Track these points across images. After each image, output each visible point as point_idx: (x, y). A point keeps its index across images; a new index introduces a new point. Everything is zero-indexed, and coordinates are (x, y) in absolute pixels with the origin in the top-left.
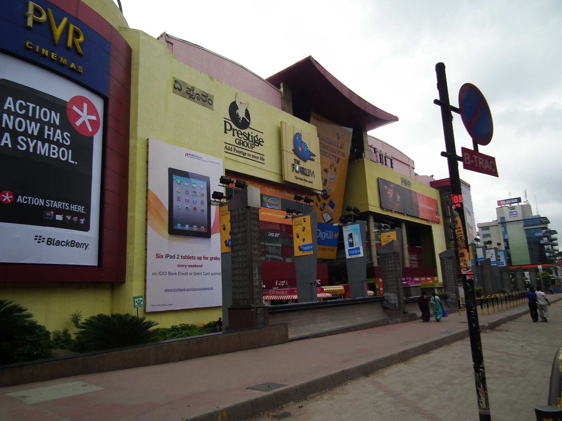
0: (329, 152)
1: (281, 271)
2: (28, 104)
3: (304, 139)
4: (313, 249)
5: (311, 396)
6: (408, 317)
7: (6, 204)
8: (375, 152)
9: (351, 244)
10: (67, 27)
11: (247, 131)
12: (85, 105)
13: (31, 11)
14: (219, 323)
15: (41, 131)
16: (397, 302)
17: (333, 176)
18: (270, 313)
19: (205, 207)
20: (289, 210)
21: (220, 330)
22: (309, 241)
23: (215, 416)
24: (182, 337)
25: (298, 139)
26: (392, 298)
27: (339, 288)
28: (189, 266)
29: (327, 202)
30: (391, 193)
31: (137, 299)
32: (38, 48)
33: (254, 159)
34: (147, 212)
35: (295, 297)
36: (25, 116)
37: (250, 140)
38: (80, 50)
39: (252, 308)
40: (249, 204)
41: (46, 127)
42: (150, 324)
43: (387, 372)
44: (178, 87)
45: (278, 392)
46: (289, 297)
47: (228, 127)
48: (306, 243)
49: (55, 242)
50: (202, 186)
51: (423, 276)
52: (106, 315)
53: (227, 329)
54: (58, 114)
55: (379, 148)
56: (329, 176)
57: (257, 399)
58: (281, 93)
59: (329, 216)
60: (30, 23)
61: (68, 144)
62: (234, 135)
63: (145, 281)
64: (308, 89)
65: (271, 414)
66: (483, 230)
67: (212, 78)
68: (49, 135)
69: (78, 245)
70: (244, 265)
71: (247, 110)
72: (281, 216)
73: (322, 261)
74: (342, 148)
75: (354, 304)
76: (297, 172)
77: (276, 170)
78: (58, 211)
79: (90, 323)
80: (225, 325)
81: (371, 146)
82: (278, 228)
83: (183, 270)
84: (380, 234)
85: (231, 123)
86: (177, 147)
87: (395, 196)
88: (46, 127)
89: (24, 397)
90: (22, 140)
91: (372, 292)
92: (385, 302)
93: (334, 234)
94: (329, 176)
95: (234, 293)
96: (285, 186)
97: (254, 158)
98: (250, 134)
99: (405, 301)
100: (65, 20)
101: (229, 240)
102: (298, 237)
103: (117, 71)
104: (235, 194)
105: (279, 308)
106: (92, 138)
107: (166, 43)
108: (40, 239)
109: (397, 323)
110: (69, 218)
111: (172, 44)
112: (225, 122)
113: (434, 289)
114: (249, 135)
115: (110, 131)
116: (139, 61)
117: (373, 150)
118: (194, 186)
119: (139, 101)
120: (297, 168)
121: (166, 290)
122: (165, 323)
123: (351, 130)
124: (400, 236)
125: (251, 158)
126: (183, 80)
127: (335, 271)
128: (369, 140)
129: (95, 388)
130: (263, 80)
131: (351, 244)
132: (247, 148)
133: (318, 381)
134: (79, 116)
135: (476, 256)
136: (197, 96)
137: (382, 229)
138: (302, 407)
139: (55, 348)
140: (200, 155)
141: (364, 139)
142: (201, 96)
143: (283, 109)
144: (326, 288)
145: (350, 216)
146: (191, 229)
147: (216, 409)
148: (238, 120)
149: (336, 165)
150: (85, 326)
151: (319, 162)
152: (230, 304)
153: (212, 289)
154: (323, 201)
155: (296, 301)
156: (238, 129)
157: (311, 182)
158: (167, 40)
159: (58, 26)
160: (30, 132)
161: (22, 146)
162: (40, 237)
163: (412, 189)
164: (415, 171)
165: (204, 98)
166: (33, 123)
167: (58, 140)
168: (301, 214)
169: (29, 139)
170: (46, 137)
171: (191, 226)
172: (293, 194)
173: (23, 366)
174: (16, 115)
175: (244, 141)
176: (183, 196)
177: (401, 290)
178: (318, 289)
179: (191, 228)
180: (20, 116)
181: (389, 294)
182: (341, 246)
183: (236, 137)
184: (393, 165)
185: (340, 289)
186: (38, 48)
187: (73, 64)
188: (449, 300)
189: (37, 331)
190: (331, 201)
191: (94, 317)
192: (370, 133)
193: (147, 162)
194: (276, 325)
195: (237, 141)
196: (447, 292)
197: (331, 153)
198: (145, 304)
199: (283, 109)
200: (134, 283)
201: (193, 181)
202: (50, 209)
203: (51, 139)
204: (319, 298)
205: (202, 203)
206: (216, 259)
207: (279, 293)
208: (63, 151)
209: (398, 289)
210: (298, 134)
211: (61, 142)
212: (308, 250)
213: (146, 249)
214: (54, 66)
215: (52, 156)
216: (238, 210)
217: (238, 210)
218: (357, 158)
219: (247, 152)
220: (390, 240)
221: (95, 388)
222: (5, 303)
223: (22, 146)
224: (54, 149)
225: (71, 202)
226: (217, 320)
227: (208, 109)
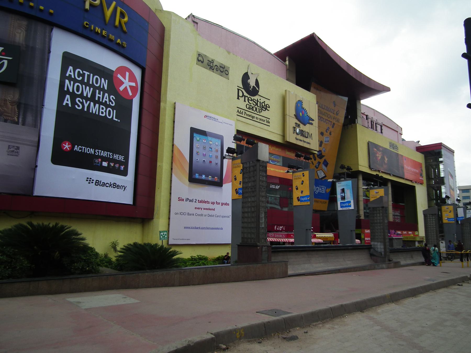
0: (326, 118)
1: (283, 218)
2: (84, 72)
4: (309, 200)
5: (314, 324)
6: (392, 264)
7: (66, 152)
8: (367, 119)
9: (343, 198)
10: (115, 9)
11: (256, 98)
12: (127, 74)
15: (94, 94)
16: (383, 250)
17: (328, 139)
18: (273, 252)
20: (291, 166)
22: (307, 192)
25: (299, 105)
26: (379, 246)
27: (330, 235)
28: (204, 209)
29: (322, 161)
30: (379, 155)
31: (162, 233)
32: (93, 26)
33: (261, 122)
34: (172, 163)
35: (292, 240)
36: (82, 82)
37: (259, 105)
38: (125, 28)
39: (258, 246)
40: (259, 158)
41: (97, 91)
42: (175, 253)
43: (380, 310)
44: (201, 60)
45: (286, 318)
46: (286, 240)
47: (241, 94)
48: (304, 194)
49: (101, 184)
51: (405, 230)
53: (236, 262)
54: (107, 81)
55: (371, 115)
56: (324, 139)
57: (269, 322)
58: (286, 65)
61: (113, 105)
62: (245, 101)
63: (169, 218)
64: (310, 62)
65: (280, 335)
66: (463, 192)
67: (229, 52)
68: (99, 97)
69: (118, 187)
71: (257, 80)
72: (282, 171)
73: (315, 211)
74: (337, 114)
75: (345, 249)
76: (297, 134)
77: (279, 132)
78: (104, 159)
79: (128, 249)
81: (363, 114)
83: (199, 212)
84: (368, 191)
85: (243, 90)
86: (200, 110)
87: (383, 158)
88: (97, 91)
89: (79, 302)
90: (79, 101)
91: (359, 241)
92: (372, 250)
94: (324, 139)
95: (243, 233)
97: (261, 121)
98: (259, 100)
100: (114, 3)
102: (297, 189)
103: (152, 45)
104: (246, 150)
105: (277, 248)
106: (132, 100)
107: (193, 24)
108: (90, 181)
110: (112, 164)
111: (197, 23)
112: (238, 90)
113: (415, 241)
114: (258, 101)
115: (146, 95)
116: (170, 37)
117: (365, 117)
118: (211, 143)
119: (169, 71)
120: (298, 131)
121: (185, 228)
122: (186, 254)
123: (346, 99)
124: (386, 193)
125: (258, 121)
127: (327, 221)
128: (360, 107)
130: (271, 54)
131: (343, 198)
132: (256, 112)
133: (320, 311)
134: (123, 83)
135: (457, 215)
136: (216, 67)
137: (371, 186)
138: (307, 332)
139: (102, 267)
140: (216, 117)
141: (358, 107)
142: (219, 67)
144: (318, 235)
145: (343, 174)
146: (206, 178)
147: (236, 327)
148: (249, 88)
149: (331, 129)
151: (317, 126)
152: (239, 241)
153: (222, 229)
154: (318, 160)
155: (292, 243)
156: (249, 96)
157: (309, 143)
158: (193, 19)
159: (108, 8)
160: (85, 95)
161: (79, 106)
162: (91, 179)
163: (400, 152)
164: (403, 137)
165: (222, 69)
166: (88, 88)
168: (301, 169)
169: (84, 101)
170: (97, 99)
171: (207, 176)
174: (75, 81)
175: (253, 106)
176: (201, 151)
177: (387, 240)
180: (78, 81)
181: (376, 243)
182: (333, 200)
183: (247, 102)
184: (383, 131)
185: (330, 236)
186: (93, 26)
187: (119, 40)
191: (130, 245)
192: (363, 102)
195: (248, 106)
198: (168, 237)
199: (287, 80)
200: (160, 220)
201: (210, 138)
202: (98, 157)
203: (101, 101)
205: (217, 157)
206: (227, 204)
207: (277, 236)
208: (110, 111)
209: (384, 239)
211: (108, 103)
212: (305, 201)
213: (171, 193)
214: (105, 42)
215: (101, 114)
218: (351, 124)
219: (256, 116)
220: (378, 197)
222: (66, 228)
223: (79, 106)
224: (103, 109)
225: (114, 152)
226: (224, 254)
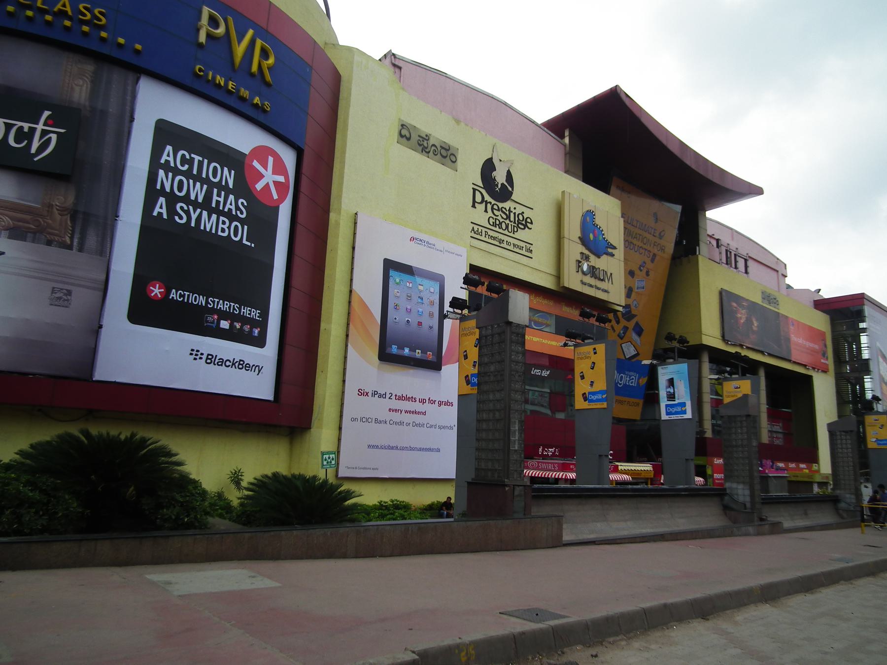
1: (555, 432)
2: (193, 155)
3: (599, 221)
4: (606, 400)
5: (611, 639)
6: (767, 527)
7: (155, 301)
8: (718, 246)
9: (671, 397)
10: (252, 43)
11: (507, 205)
12: (271, 160)
13: (205, 20)
14: (447, 505)
16: (748, 499)
17: (643, 284)
18: (534, 497)
19: (435, 322)
20: (571, 333)
21: (448, 516)
22: (601, 385)
23: (457, 651)
24: (394, 519)
25: (588, 221)
26: (741, 492)
28: (406, 412)
29: (631, 324)
30: (742, 315)
33: (515, 250)
34: (348, 324)
35: (572, 475)
36: (188, 174)
37: (512, 219)
38: (268, 78)
39: (506, 485)
40: (511, 320)
41: (215, 190)
42: (349, 495)
44: (407, 135)
45: (556, 626)
47: (478, 198)
48: (596, 388)
50: (432, 290)
52: (284, 474)
53: (464, 515)
54: (233, 172)
55: (725, 239)
56: (636, 283)
57: (523, 633)
58: (565, 145)
59: (632, 349)
60: (202, 38)
61: (243, 216)
62: (486, 211)
63: (340, 428)
64: (610, 140)
67: (458, 121)
68: (218, 202)
70: (497, 415)
72: (554, 343)
73: (618, 421)
74: (661, 237)
75: (673, 496)
76: (584, 273)
78: (224, 315)
80: (461, 507)
81: (710, 237)
82: (546, 362)
83: (396, 417)
84: (721, 384)
85: (484, 191)
86: (404, 229)
87: (749, 321)
88: (215, 190)
89: (170, 583)
90: (182, 208)
91: (701, 479)
92: (726, 498)
93: (639, 379)
94: (636, 283)
95: (478, 459)
96: (564, 296)
97: (516, 249)
98: (512, 209)
99: (763, 499)
100: (250, 32)
101: (472, 375)
102: (583, 377)
103: (317, 107)
105: (543, 491)
107: (392, 69)
108: (196, 355)
109: (747, 534)
110: (238, 326)
111: (400, 68)
112: (474, 190)
114: (510, 211)
115: (303, 199)
117: (714, 243)
118: (421, 288)
119: (347, 155)
120: (585, 268)
122: (369, 496)
123: (678, 208)
124: (755, 388)
125: (511, 248)
126: (414, 123)
129: (268, 583)
130: (536, 124)
131: (671, 397)
132: (506, 232)
136: (433, 148)
137: (726, 375)
138: (596, 656)
139: (212, 516)
140: (432, 240)
141: (701, 224)
142: (439, 148)
143: (567, 172)
144: (623, 466)
145: (672, 350)
147: (459, 641)
148: (495, 187)
149: (649, 265)
150: (254, 487)
151: (622, 258)
152: (471, 476)
153: (438, 450)
154: (623, 323)
155: (572, 481)
156: (493, 202)
158: (394, 62)
159: (240, 41)
160: (193, 197)
161: (181, 218)
162: (198, 351)
165: (444, 153)
166: (198, 184)
167: (230, 210)
169: (191, 208)
170: (214, 205)
171: (413, 350)
172: (576, 308)
173: (168, 536)
174: (176, 172)
175: (501, 220)
176: (404, 304)
177: (757, 481)
178: (610, 466)
179: (412, 353)
181: (734, 485)
182: (651, 398)
183: (490, 214)
184: (749, 270)
185: (646, 469)
187: (257, 98)
188: (842, 505)
189: (190, 487)
190: (637, 324)
191: (266, 476)
192: (710, 214)
193: (354, 248)
194: (544, 517)
195: (491, 221)
196: (838, 492)
197: (641, 245)
198: (338, 464)
199: (566, 172)
201: (419, 280)
202: (213, 311)
204: (612, 482)
205: (431, 315)
206: (448, 404)
207: (544, 466)
210: (589, 211)
211: (234, 213)
213: (344, 381)
215: (220, 233)
216: (492, 327)
217: (492, 327)
218: (686, 256)
219: (501, 237)
220: (740, 395)
221: (268, 583)
223: (181, 218)
224: (224, 223)
225: (242, 303)
227: (449, 170)
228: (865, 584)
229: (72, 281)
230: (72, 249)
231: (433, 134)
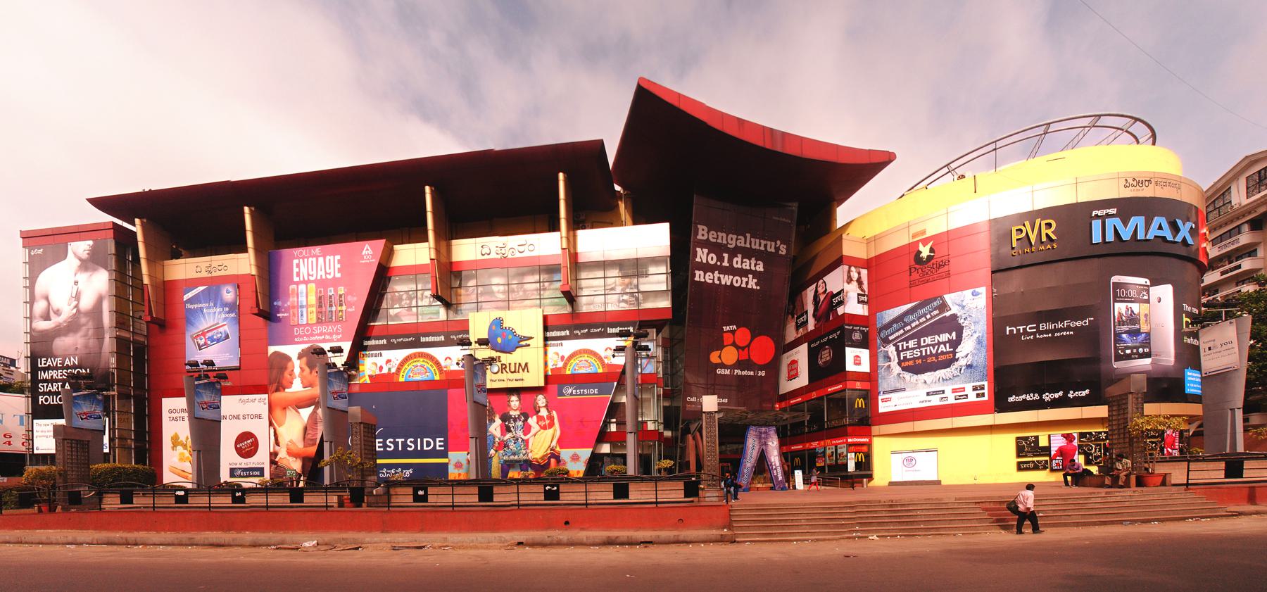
33: (993, 146)
123: (667, 225)
198: (304, 209)
228: (1062, 264)
229: (430, 339)
230: (1018, 456)
231: (1205, 437)
